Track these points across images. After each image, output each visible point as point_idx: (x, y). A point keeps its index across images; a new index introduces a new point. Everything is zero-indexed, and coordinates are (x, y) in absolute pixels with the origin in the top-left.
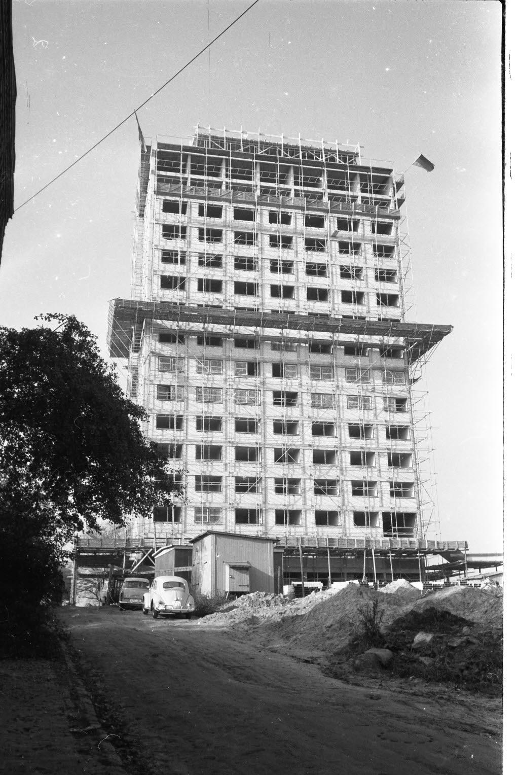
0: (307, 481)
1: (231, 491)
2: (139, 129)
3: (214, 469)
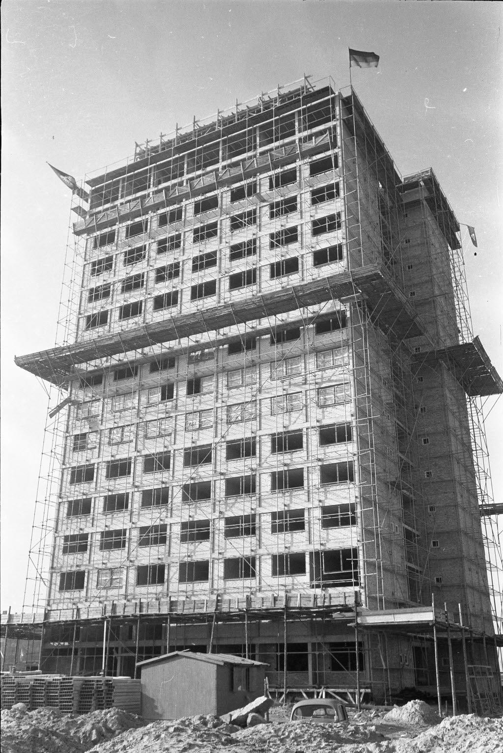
0: (216, 521)
1: (317, 526)
2: (60, 173)
3: (297, 500)
